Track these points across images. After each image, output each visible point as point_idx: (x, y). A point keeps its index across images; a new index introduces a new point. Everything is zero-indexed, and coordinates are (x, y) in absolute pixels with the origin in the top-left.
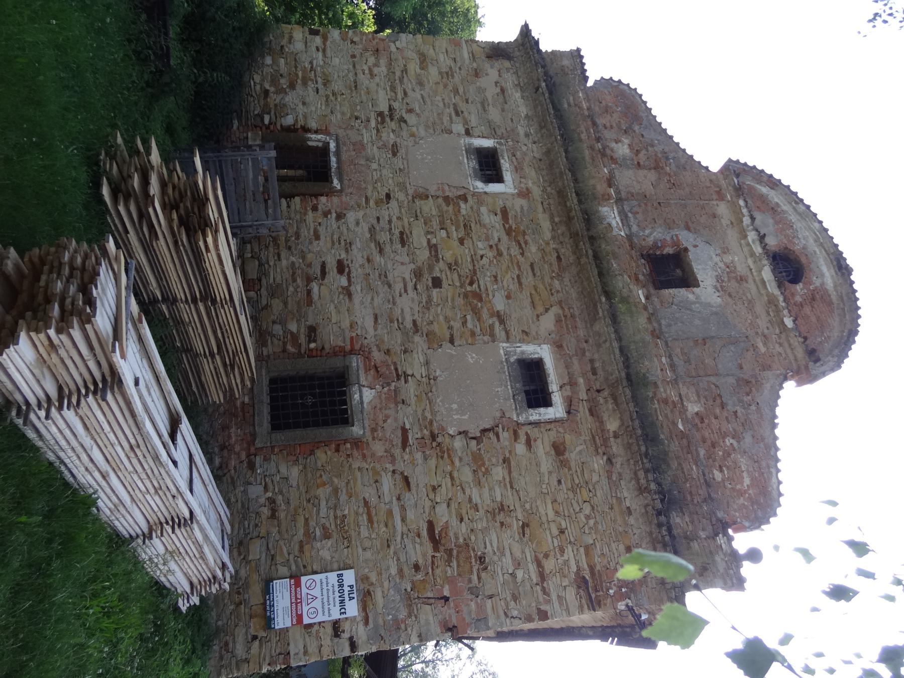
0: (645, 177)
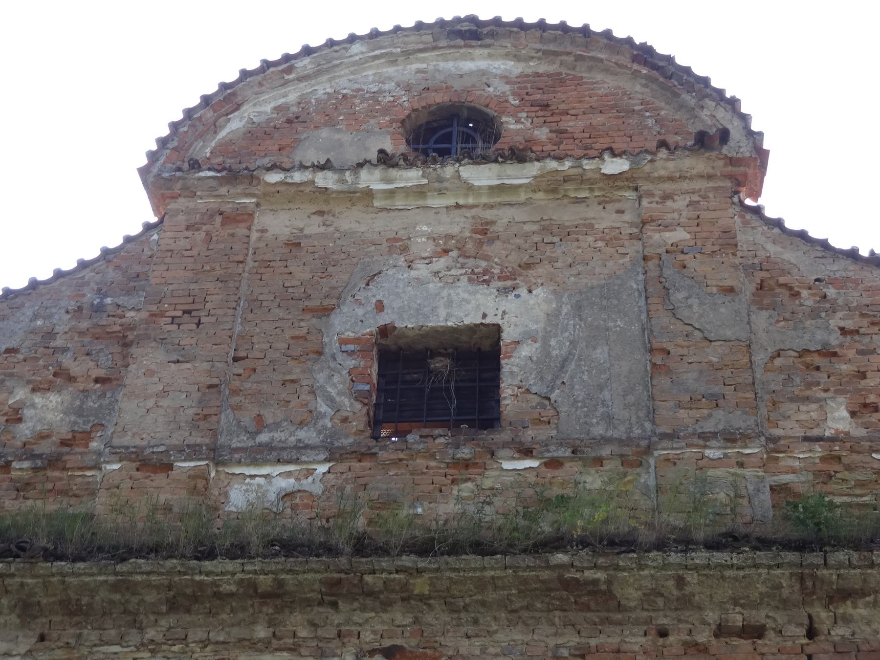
0: (150, 373)
